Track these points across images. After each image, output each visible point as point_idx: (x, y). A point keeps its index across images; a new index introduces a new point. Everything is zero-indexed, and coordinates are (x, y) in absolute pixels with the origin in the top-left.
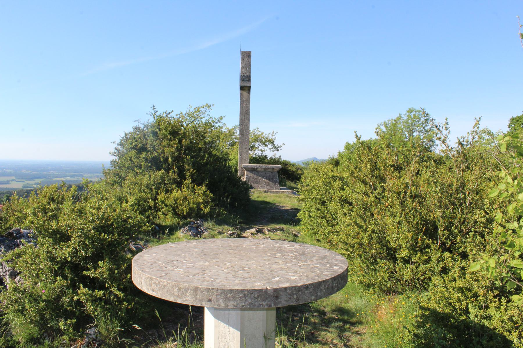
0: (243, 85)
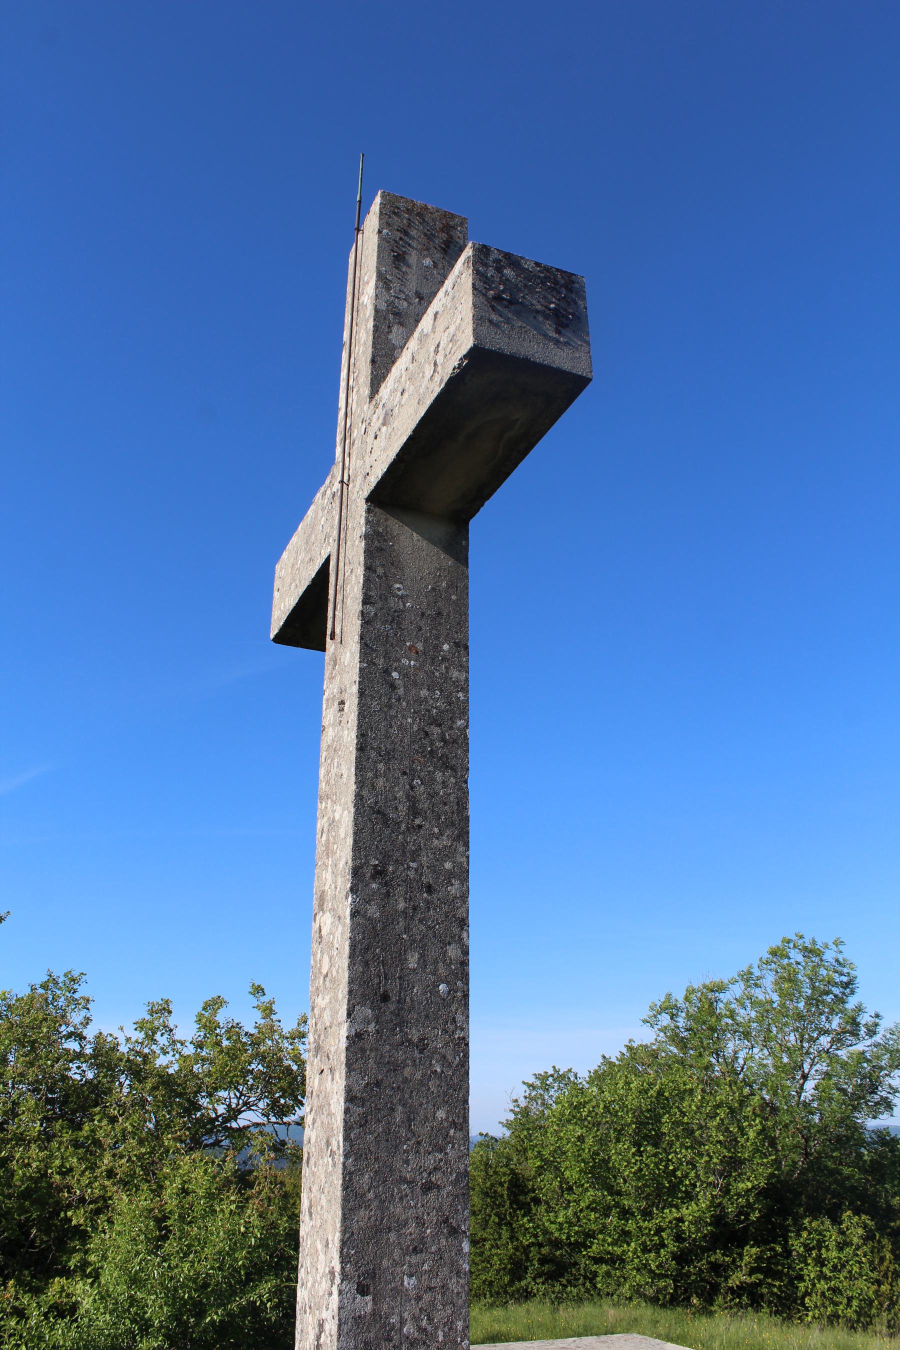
0: (500, 342)
